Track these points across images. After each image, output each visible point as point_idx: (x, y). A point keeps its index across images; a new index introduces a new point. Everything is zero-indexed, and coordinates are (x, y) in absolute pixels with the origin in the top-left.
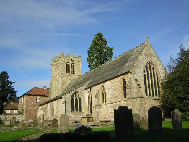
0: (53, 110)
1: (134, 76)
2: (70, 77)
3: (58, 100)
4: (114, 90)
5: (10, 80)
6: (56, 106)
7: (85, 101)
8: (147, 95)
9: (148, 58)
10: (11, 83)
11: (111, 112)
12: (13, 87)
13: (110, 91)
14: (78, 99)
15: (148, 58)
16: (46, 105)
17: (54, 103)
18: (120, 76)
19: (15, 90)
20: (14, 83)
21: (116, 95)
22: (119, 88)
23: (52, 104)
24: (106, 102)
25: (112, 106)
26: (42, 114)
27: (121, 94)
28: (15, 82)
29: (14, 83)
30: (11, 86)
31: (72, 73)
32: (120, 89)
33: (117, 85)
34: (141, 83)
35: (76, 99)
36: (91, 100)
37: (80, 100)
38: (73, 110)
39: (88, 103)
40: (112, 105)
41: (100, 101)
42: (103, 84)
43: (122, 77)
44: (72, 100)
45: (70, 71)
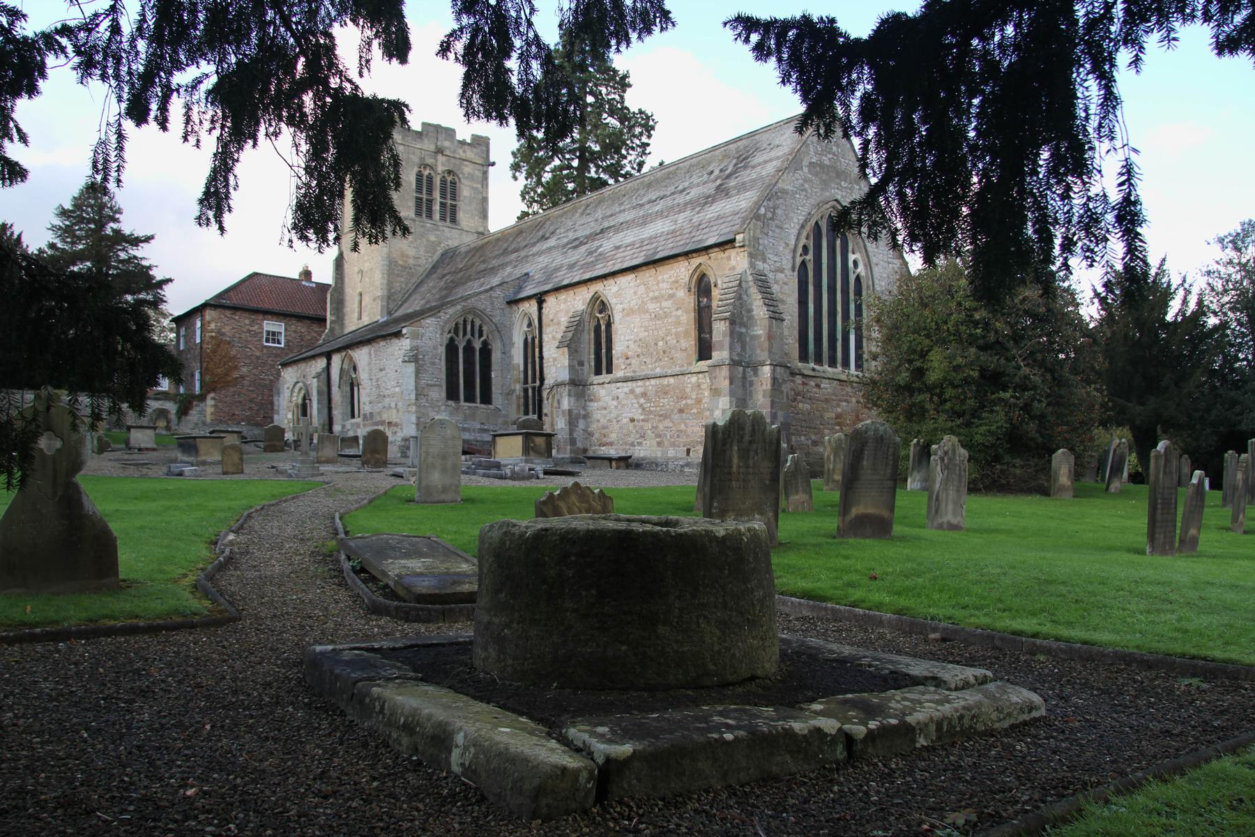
0: (353, 385)
1: (752, 265)
2: (433, 238)
3: (382, 343)
4: (651, 320)
5: (128, 224)
6: (370, 370)
7: (511, 357)
8: (804, 357)
9: (825, 184)
10: (136, 241)
11: (632, 420)
12: (145, 263)
13: (636, 320)
14: (477, 345)
15: (825, 184)
16: (321, 363)
17: (361, 356)
18: (687, 254)
19: (158, 274)
20: (148, 239)
21: (660, 344)
22: (679, 312)
23: (351, 359)
24: (609, 371)
25: (638, 391)
26: (300, 401)
27: (684, 344)
28: (152, 237)
29: (148, 239)
30: (135, 257)
31: (443, 218)
32: (684, 319)
33: (671, 296)
34: (783, 302)
35: (469, 349)
36: (541, 358)
37: (486, 352)
38: (452, 394)
39: (522, 368)
40: (638, 387)
41: (581, 364)
42: (597, 287)
43: (696, 261)
44: (451, 348)
45: (437, 207)
